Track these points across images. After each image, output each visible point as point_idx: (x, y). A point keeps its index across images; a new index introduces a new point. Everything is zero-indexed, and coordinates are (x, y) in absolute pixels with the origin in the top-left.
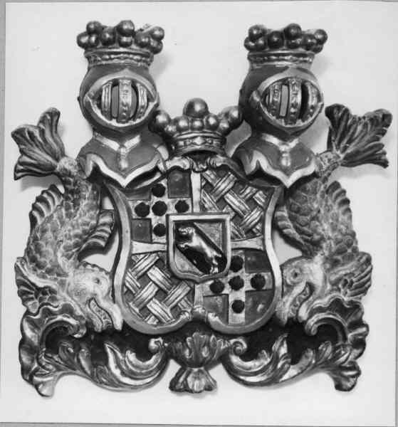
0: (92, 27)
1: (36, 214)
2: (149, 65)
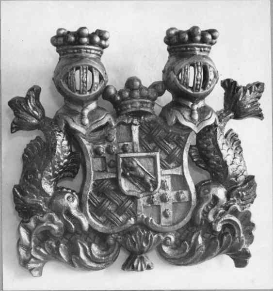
0: (62, 32)
1: (162, 163)
2: (100, 56)
